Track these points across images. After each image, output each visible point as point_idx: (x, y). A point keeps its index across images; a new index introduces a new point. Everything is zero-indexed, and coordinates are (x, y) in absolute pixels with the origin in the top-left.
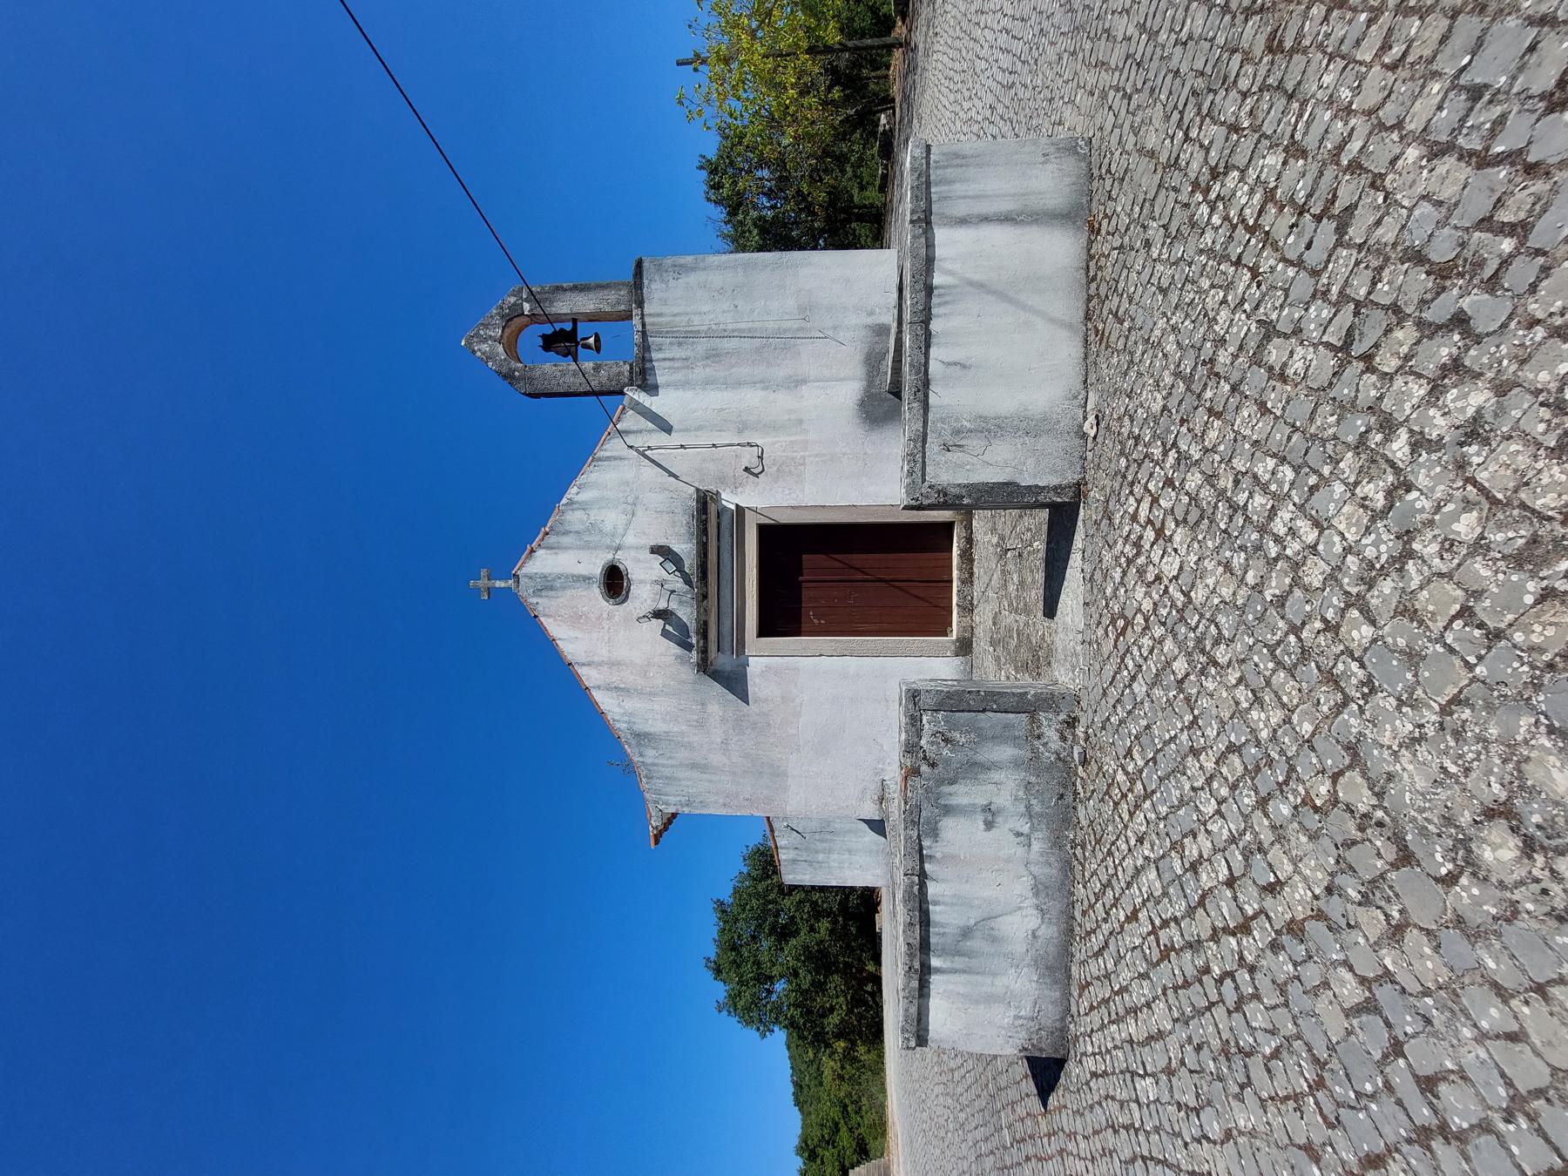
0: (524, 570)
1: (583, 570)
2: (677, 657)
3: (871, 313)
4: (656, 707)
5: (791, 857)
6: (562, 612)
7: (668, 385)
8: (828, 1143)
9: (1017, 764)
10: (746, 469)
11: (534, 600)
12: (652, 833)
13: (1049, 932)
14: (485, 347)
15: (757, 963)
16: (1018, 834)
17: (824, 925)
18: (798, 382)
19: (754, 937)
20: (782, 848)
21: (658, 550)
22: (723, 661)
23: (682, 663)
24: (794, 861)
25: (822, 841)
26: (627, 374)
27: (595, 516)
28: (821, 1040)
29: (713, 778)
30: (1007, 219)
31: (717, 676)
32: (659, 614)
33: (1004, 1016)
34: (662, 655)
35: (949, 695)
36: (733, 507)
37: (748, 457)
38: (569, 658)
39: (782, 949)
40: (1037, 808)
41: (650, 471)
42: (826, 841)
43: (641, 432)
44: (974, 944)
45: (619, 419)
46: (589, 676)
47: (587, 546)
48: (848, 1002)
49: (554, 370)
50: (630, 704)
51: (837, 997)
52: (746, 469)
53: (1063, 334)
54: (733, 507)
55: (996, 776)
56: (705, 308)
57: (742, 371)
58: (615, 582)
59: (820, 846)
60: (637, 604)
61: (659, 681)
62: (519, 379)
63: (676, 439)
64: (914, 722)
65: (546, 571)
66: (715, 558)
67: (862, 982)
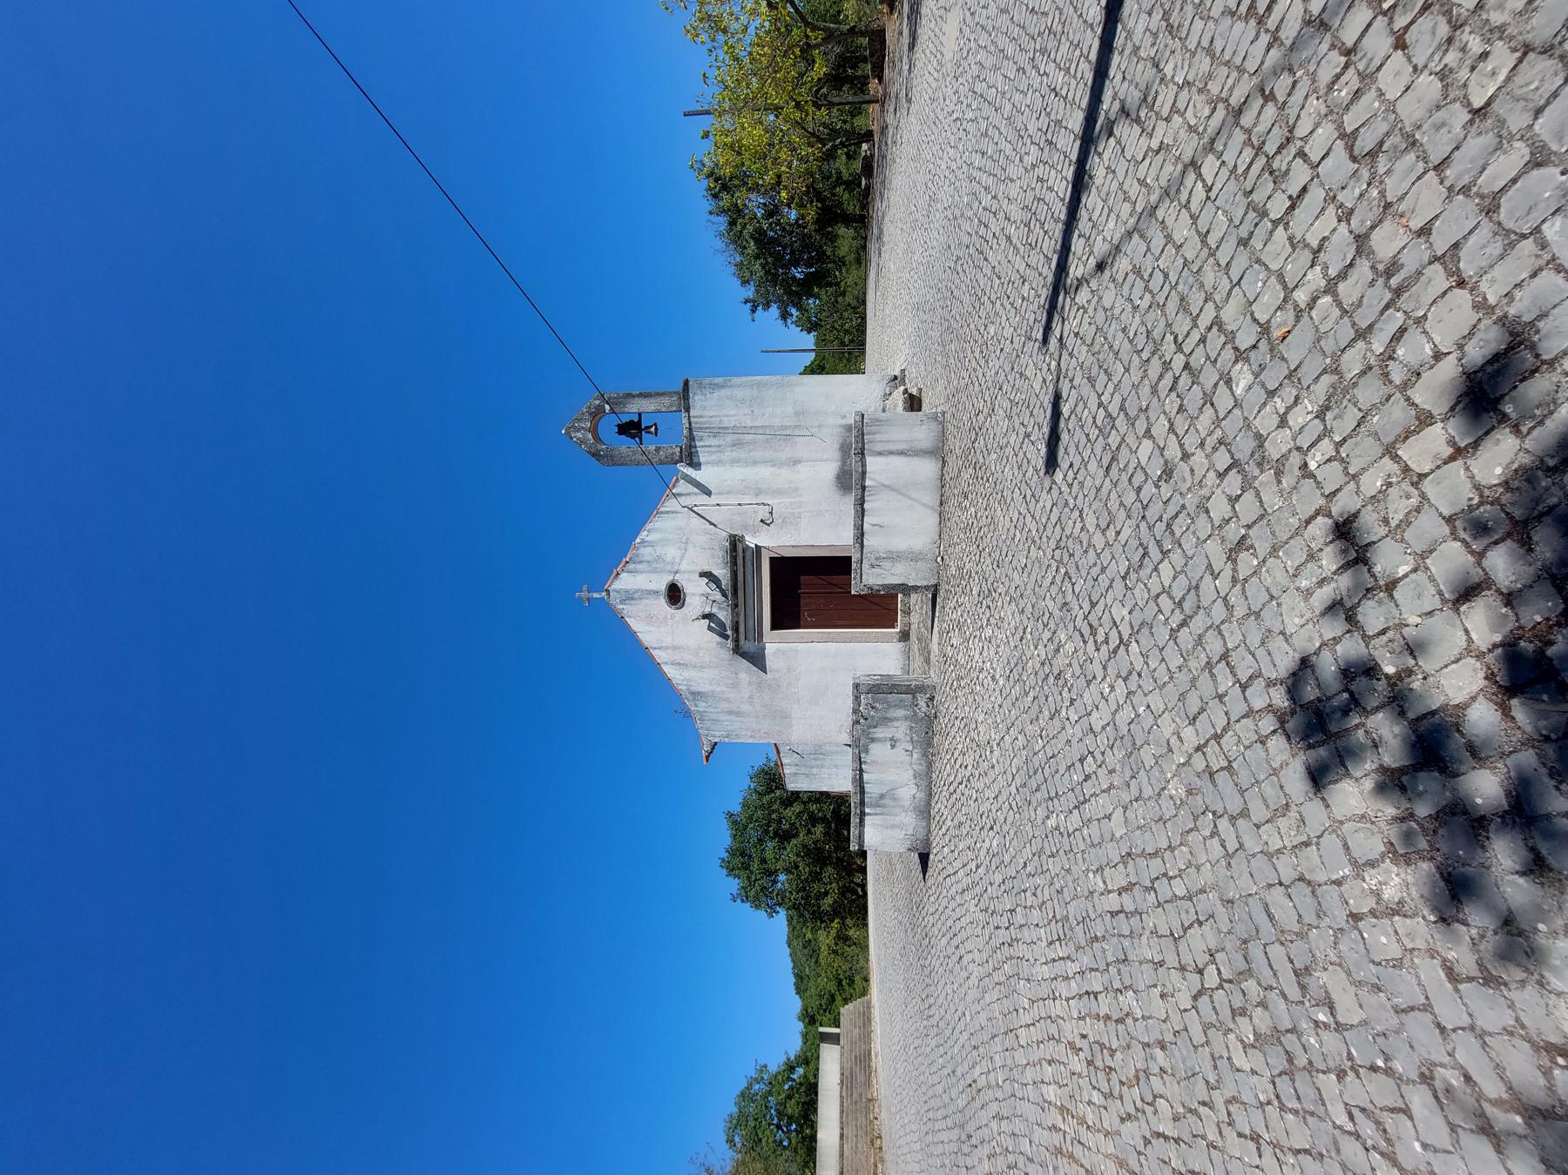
0: (613, 587)
1: (654, 587)
2: (718, 643)
4: (705, 675)
6: (640, 614)
8: (825, 1011)
9: (906, 718)
10: (762, 521)
11: (620, 607)
12: (704, 754)
13: (921, 795)
14: (579, 435)
15: (763, 861)
16: (907, 751)
17: (819, 830)
18: (797, 462)
19: (760, 840)
21: (703, 574)
22: (747, 646)
23: (721, 647)
24: (795, 774)
26: (678, 454)
27: (659, 550)
28: (819, 917)
30: (902, 453)
31: (744, 655)
32: (705, 616)
33: (899, 834)
34: (708, 642)
35: (874, 686)
36: (753, 546)
37: (763, 513)
38: (646, 644)
39: (785, 848)
40: (915, 738)
41: (696, 521)
42: (819, 759)
43: (689, 494)
44: (886, 801)
45: (674, 486)
46: (660, 656)
47: (654, 571)
48: (839, 888)
49: (625, 445)
51: (831, 884)
52: (762, 521)
53: (929, 511)
54: (753, 546)
55: (896, 724)
56: (733, 412)
57: (757, 454)
58: (675, 595)
59: (814, 763)
60: (691, 609)
61: (707, 659)
62: (603, 456)
63: (714, 499)
64: (857, 698)
65: (628, 587)
67: (850, 873)
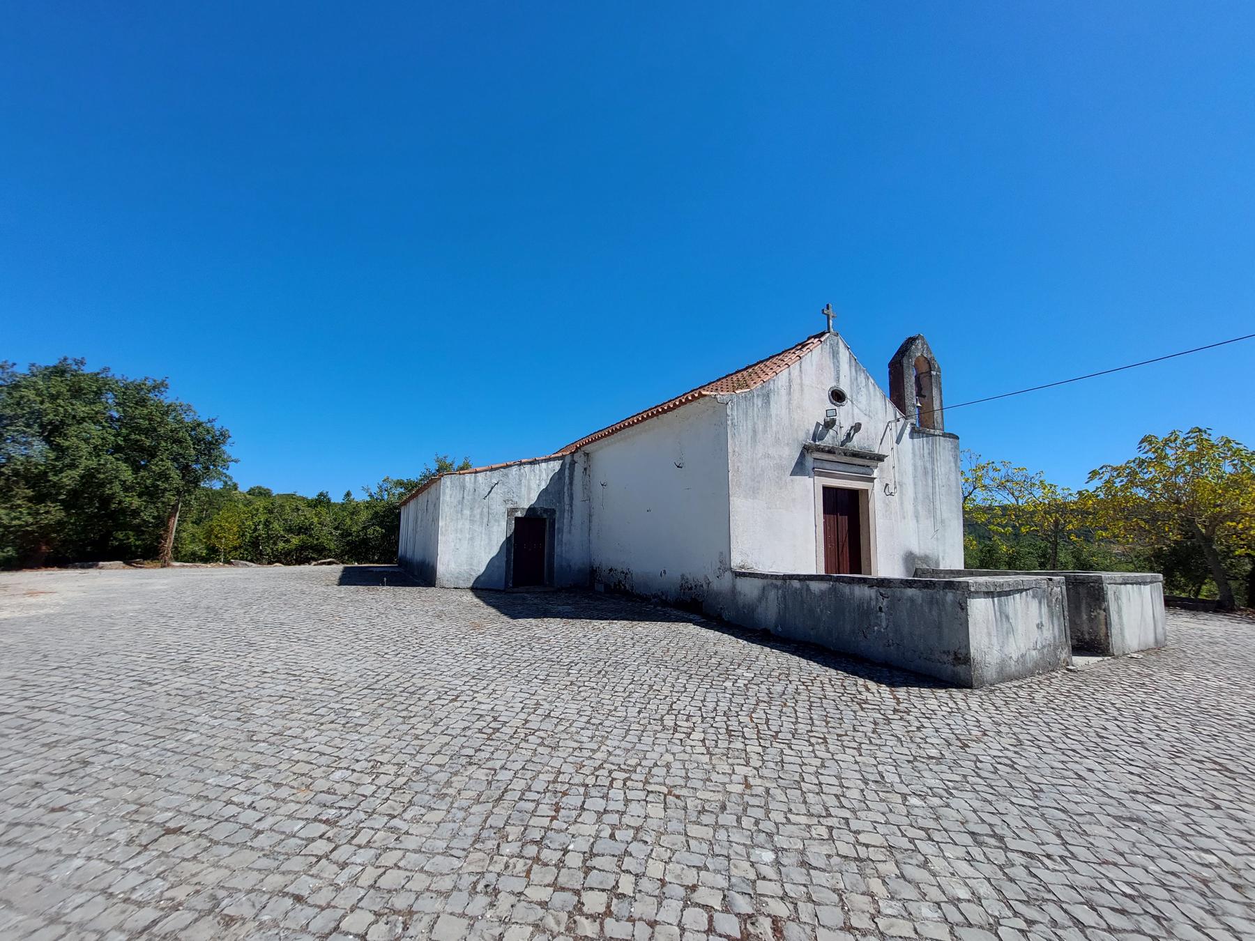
3: (943, 559)
4: (784, 411)
5: (467, 485)
7: (913, 445)
20: (475, 477)
24: (463, 488)
25: (482, 514)
29: (749, 445)
42: (482, 518)
47: (852, 383)
50: (783, 392)
59: (477, 511)
65: (841, 355)
66: (855, 462)
